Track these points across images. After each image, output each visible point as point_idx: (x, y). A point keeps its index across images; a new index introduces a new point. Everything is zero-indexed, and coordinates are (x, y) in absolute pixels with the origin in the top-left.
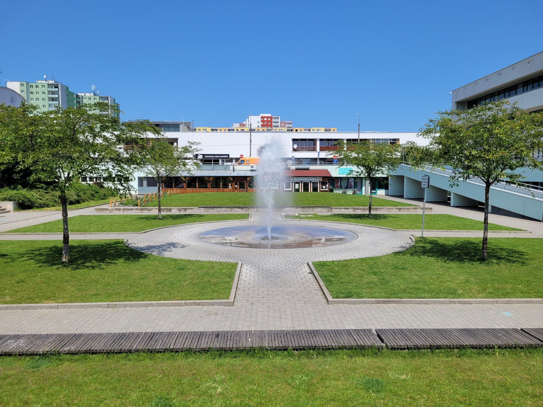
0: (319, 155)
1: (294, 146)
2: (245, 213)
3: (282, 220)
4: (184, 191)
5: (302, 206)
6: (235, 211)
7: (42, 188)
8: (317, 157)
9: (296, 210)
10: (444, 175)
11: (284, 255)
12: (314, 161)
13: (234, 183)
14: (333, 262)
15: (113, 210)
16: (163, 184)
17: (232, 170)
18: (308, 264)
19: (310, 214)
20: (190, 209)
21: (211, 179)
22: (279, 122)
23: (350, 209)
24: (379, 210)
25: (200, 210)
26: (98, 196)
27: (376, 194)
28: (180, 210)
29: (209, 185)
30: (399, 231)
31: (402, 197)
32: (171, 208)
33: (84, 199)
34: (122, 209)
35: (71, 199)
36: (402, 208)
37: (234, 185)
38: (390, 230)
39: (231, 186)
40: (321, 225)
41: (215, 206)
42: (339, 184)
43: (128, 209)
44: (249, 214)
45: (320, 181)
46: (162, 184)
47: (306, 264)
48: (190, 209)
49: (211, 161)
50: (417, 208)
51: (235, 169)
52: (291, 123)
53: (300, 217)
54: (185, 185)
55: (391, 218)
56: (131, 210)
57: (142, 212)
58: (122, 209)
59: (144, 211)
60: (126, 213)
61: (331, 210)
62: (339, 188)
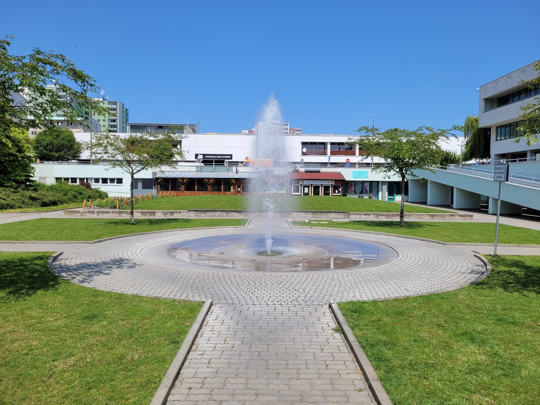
0: (329, 159)
1: (303, 150)
2: (244, 218)
3: (289, 227)
4: (181, 194)
5: (313, 211)
6: (231, 216)
7: (11, 187)
8: (327, 161)
9: (305, 215)
10: (480, 177)
11: (288, 284)
12: (325, 164)
13: (237, 186)
14: (375, 302)
15: (85, 212)
16: (159, 186)
17: (235, 172)
18: (330, 306)
19: (324, 221)
20: (178, 212)
21: (185, 181)
22: (288, 129)
23: (372, 215)
24: (407, 216)
25: (189, 214)
26: (81, 198)
27: (394, 200)
28: (165, 214)
29: (209, 188)
30: (451, 244)
31: (425, 203)
32: (155, 211)
33: (62, 200)
34: (96, 212)
35: (44, 201)
36: (436, 215)
37: (237, 188)
38: (437, 242)
39: (234, 189)
40: (340, 235)
41: (208, 210)
42: (353, 188)
43: (103, 212)
44: (247, 220)
45: (332, 185)
46: (157, 187)
47: (327, 306)
48: (178, 212)
49: (212, 162)
50: (454, 215)
51: (238, 171)
52: (300, 130)
53: (311, 223)
54: (183, 187)
55: (429, 227)
56: (107, 212)
57: (120, 216)
58: (96, 212)
59: (122, 215)
60: (102, 216)
61: (349, 216)
62: (353, 192)
